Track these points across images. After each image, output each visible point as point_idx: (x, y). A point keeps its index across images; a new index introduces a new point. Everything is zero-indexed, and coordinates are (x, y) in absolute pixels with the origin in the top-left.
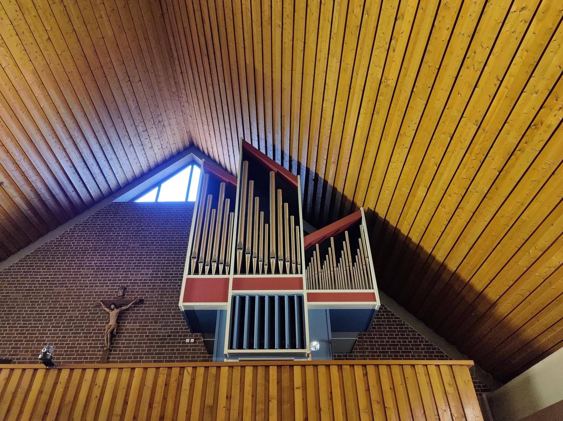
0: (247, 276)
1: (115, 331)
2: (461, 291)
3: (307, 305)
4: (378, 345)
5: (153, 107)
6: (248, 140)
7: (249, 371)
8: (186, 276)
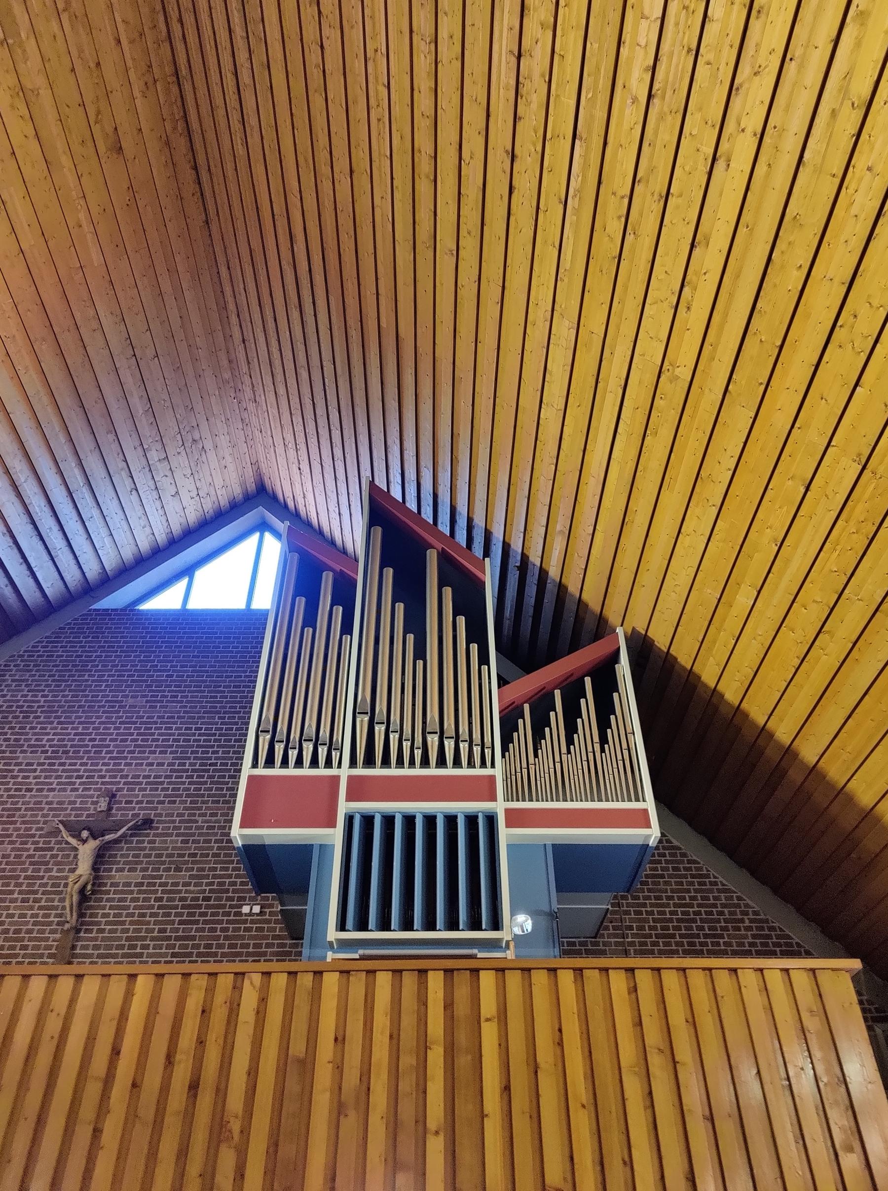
0: (378, 771)
1: (89, 887)
2: (828, 807)
3: (504, 834)
4: (654, 920)
5: (180, 411)
6: (381, 483)
7: (384, 980)
8: (247, 770)
